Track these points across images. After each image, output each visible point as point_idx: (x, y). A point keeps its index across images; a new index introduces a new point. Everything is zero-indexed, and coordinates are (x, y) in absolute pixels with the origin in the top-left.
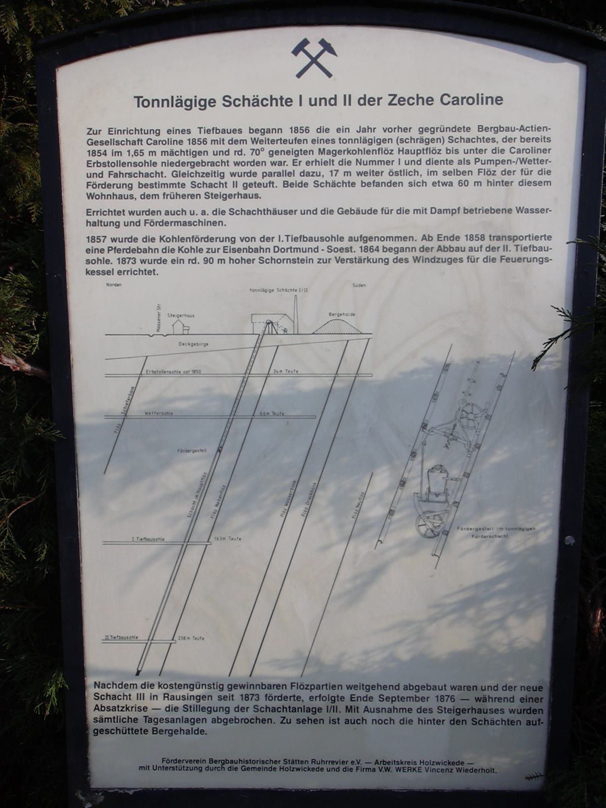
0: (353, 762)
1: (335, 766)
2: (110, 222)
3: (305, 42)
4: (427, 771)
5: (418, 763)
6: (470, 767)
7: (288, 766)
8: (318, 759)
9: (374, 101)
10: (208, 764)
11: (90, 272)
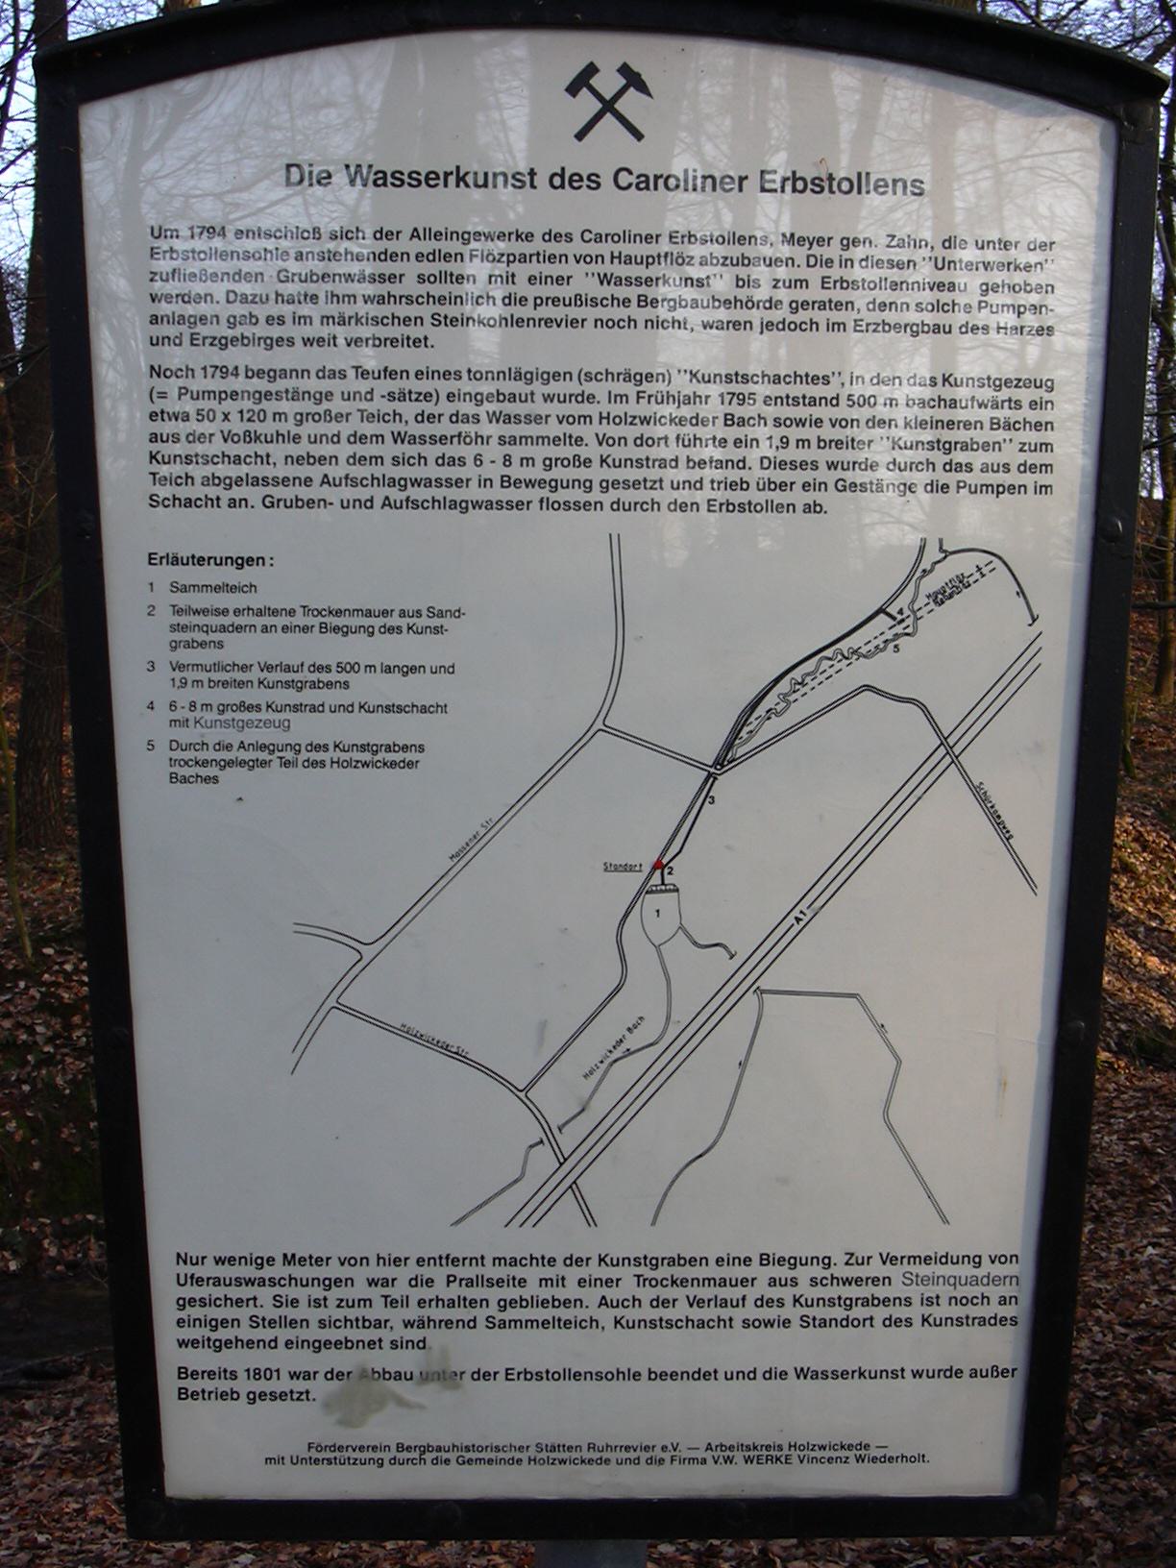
0: (664, 1448)
1: (632, 1455)
2: (227, 558)
3: (591, 70)
4: (802, 1462)
5: (786, 1447)
6: (879, 1453)
7: (544, 1455)
8: (600, 1443)
9: (438, 178)
10: (393, 1453)
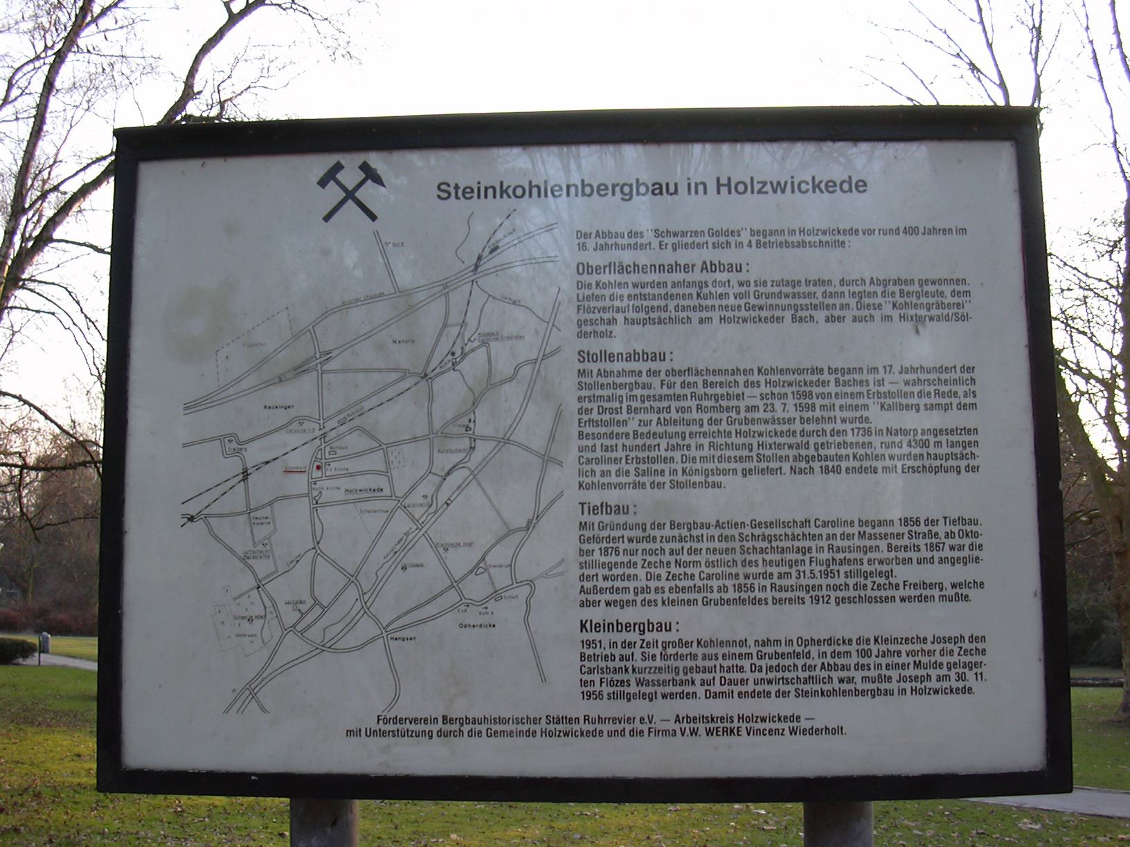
1: (619, 727)
11: (823, 186)
